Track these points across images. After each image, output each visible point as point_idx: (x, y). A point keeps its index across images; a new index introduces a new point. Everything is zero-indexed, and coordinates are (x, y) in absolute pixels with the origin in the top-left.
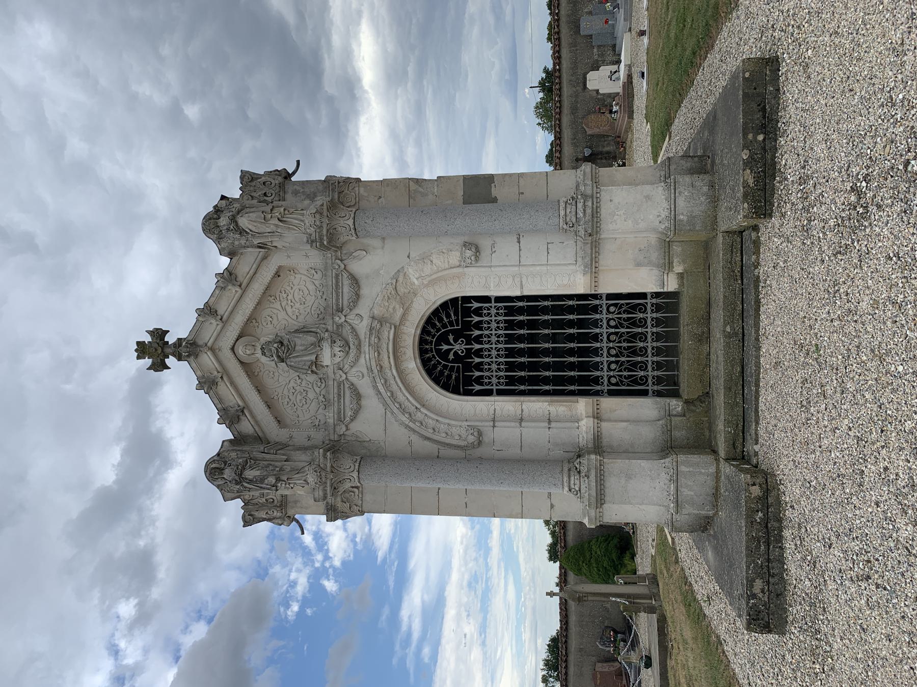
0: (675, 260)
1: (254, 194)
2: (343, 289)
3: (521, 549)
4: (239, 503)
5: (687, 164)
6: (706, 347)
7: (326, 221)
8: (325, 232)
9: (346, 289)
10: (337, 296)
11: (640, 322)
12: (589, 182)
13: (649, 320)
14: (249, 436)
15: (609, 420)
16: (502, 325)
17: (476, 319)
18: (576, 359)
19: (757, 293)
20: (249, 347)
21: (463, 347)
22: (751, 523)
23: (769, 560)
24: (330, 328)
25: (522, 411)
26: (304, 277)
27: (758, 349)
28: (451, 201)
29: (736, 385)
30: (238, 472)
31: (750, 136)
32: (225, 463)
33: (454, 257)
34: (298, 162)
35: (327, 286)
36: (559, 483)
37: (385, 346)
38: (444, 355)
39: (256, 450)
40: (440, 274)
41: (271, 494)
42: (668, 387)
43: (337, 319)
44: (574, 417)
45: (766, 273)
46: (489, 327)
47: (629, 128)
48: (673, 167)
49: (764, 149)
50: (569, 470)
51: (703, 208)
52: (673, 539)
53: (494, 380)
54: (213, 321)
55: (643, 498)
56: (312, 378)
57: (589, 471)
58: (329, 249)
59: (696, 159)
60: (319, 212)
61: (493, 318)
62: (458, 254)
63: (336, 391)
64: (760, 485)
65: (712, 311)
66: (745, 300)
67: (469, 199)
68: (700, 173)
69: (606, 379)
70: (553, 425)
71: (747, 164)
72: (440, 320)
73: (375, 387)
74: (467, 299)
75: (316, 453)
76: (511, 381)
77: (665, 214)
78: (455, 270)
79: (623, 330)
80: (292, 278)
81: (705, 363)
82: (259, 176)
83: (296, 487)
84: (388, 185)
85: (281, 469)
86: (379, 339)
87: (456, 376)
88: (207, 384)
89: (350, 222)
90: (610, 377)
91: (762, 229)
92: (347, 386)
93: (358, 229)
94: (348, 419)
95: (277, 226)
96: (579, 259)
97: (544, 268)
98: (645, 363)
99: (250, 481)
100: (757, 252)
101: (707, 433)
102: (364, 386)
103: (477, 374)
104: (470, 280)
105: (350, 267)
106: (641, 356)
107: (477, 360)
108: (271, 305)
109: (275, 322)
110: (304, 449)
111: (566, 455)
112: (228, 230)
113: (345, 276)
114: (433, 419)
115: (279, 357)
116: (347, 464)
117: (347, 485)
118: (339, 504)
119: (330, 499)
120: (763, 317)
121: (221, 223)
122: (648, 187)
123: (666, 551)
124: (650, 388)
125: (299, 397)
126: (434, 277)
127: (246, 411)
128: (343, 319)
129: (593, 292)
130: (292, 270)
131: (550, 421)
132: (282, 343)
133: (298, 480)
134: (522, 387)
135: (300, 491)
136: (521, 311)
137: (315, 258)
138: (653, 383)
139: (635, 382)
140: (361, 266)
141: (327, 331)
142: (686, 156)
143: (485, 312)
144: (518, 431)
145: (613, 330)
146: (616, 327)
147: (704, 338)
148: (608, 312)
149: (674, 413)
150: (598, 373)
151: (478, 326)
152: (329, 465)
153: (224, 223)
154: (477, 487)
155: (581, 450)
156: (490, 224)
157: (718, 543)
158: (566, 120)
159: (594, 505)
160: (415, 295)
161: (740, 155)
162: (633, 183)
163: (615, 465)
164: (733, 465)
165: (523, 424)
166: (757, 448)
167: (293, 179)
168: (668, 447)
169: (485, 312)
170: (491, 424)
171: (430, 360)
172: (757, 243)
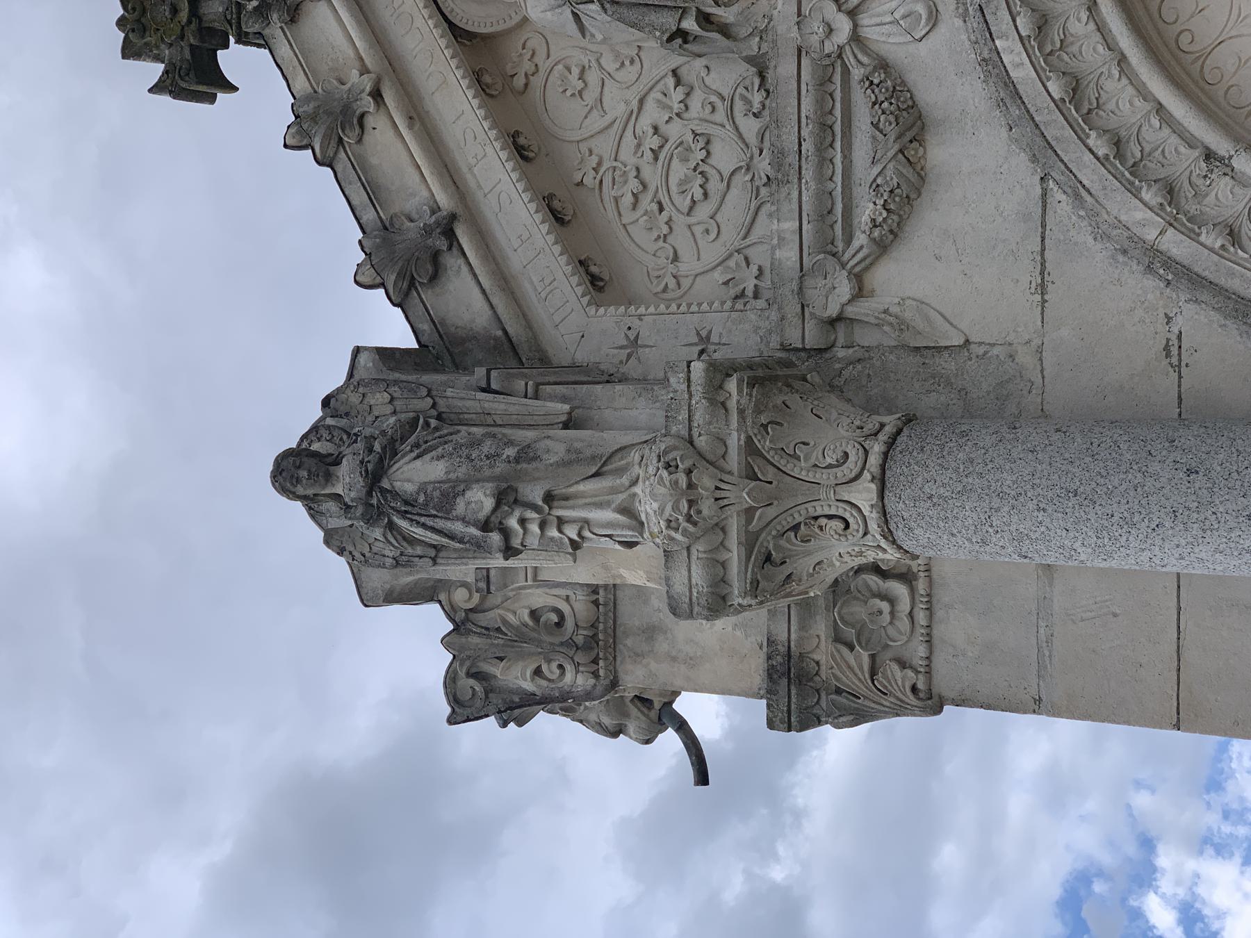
4: (428, 623)
63: (807, 105)
73: (993, 66)
85: (526, 454)
92: (857, 73)
94: (860, 239)
118: (823, 653)
125: (679, 170)
152: (734, 441)
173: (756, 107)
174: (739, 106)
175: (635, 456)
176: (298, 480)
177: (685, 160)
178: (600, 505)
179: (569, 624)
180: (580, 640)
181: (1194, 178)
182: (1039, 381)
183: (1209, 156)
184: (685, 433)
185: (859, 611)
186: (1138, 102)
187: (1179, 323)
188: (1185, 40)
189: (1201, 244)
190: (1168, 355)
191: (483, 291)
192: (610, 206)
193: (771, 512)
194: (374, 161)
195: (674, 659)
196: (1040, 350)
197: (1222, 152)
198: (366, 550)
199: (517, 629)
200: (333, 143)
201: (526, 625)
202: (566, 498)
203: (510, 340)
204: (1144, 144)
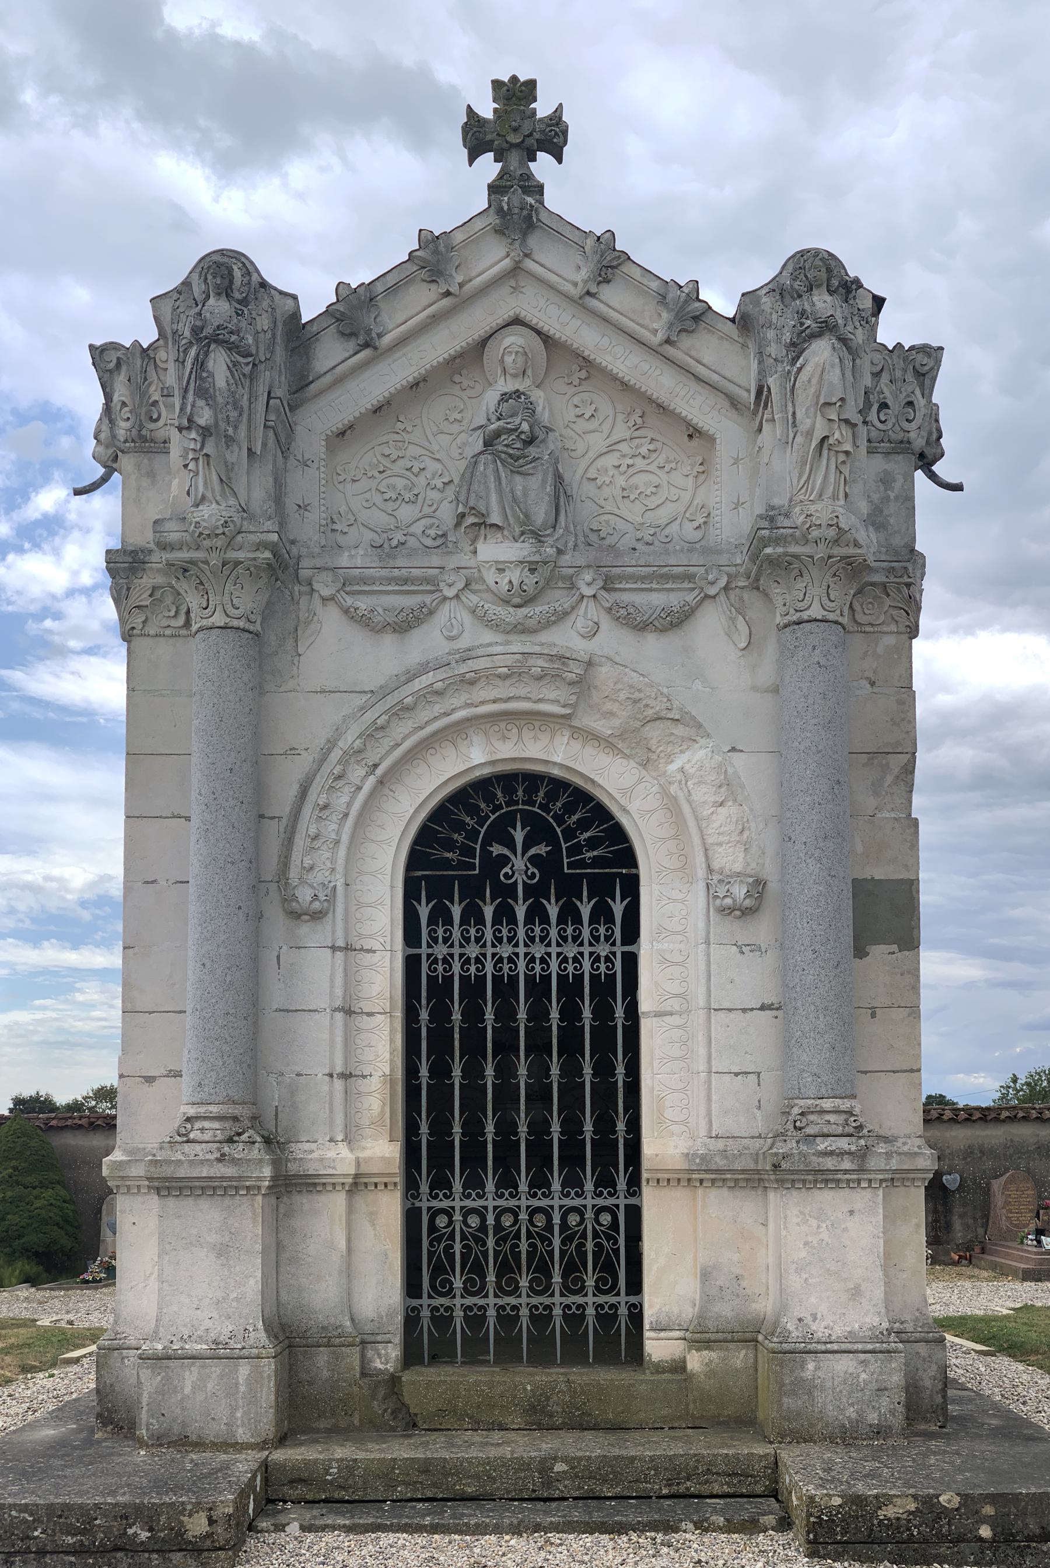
0: (713, 1355)
1: (885, 378)
2: (658, 589)
3: (39, 1015)
4: (148, 334)
5: (928, 1380)
6: (518, 1421)
7: (820, 552)
8: (794, 549)
9: (658, 600)
10: (643, 578)
12: (894, 1164)
13: (579, 1300)
14: (309, 361)
15: (350, 1210)
16: (570, 969)
17: (585, 910)
18: (490, 1138)
19: (640, 1528)
20: (520, 360)
21: (520, 878)
22: (126, 1515)
23: (42, 1553)
24: (566, 559)
25: (370, 1014)
26: (686, 497)
27: (516, 1531)
28: (860, 849)
29: (434, 1485)
30: (224, 335)
31: (989, 1510)
32: (244, 302)
33: (730, 858)
34: (958, 487)
35: (667, 552)
36: (204, 1096)
37: (522, 691)
38: (501, 833)
39: (274, 378)
41: (169, 416)
43: (588, 578)
44: (357, 1134)
45: (686, 1545)
46: (565, 939)
47: (1002, 1272)
48: (922, 1349)
49: (960, 1539)
50: (235, 1119)
51: (831, 1412)
52: (77, 1360)
53: (440, 951)
54: (583, 274)
55: (177, 1285)
56: (447, 514)
57: (235, 1161)
58: (754, 558)
59: (939, 1399)
60: (841, 536)
62: (738, 867)
63: (416, 572)
64: (209, 1535)
65: (601, 1433)
66: (624, 1503)
67: (865, 892)
68: (908, 1407)
69: (445, 1204)
70: (339, 1084)
71: (929, 1503)
72: (584, 825)
73: (425, 668)
74: (632, 888)
75: (268, 525)
77: (819, 1329)
78: (700, 859)
79: (557, 1242)
80: (686, 469)
81: (484, 1420)
82: (927, 391)
83: (187, 476)
84: (901, 702)
85: (230, 440)
86: (540, 678)
88: (433, 257)
89: (816, 612)
90: (448, 1213)
91: (782, 1538)
92: (428, 599)
93: (799, 630)
94: (349, 601)
95: (810, 433)
96: (720, 1144)
97: (702, 1066)
98: (481, 1291)
99: (200, 364)
100: (730, 1528)
101: (323, 1424)
102: (428, 642)
103: (456, 911)
104: (676, 894)
105: (709, 608)
107: (488, 911)
108: (620, 417)
109: (582, 425)
110: (278, 497)
111: (270, 1113)
112: (802, 314)
113: (690, 597)
114: (349, 805)
115: (497, 434)
116: (246, 599)
117: (193, 600)
118: (147, 581)
119: (159, 558)
120: (588, 1539)
121: (820, 294)
122: (879, 1293)
123: (48, 1349)
124: (425, 1301)
127: (366, 353)
128: (588, 591)
129: (645, 1175)
130: (705, 469)
131: (346, 1076)
132: (530, 441)
133: (205, 480)
134: (424, 1015)
135: (177, 485)
136: (603, 1013)
137: (733, 525)
138: (436, 1309)
139: (438, 1270)
140: (711, 627)
141: (560, 552)
142: (946, 1382)
144: (323, 1003)
145: (557, 1220)
146: (564, 1226)
147: (539, 1418)
148: (599, 1211)
149: (370, 1354)
150: (457, 1186)
151: (569, 914)
152: (240, 555)
153: (819, 305)
154: (193, 909)
155: (282, 1146)
156: (807, 942)
157: (75, 1448)
158: (1025, 1132)
159: (157, 1172)
160: (644, 766)
161: (949, 1488)
162: (889, 1262)
163: (248, 1220)
164: (254, 1477)
165: (339, 1016)
166: (294, 1528)
167: (919, 475)
168: (291, 1338)
169: (602, 930)
170: (340, 943)
171: (490, 798)
172: (751, 1527)
173: (428, 532)
174: (430, 521)
175: (232, 502)
176: (214, 277)
177: (405, 488)
178: (205, 483)
179: (152, 426)
180: (144, 432)
182: (281, 690)
183: (376, 766)
184: (243, 529)
185: (169, 600)
186: (402, 735)
187: (304, 754)
188: (432, 751)
191: (334, 367)
192: (384, 439)
193: (208, 573)
194: (411, 290)
195: (138, 490)
196: (294, 690)
198: (181, 310)
199: (147, 391)
200: (422, 264)
201: (149, 398)
202: (208, 464)
203: (307, 385)
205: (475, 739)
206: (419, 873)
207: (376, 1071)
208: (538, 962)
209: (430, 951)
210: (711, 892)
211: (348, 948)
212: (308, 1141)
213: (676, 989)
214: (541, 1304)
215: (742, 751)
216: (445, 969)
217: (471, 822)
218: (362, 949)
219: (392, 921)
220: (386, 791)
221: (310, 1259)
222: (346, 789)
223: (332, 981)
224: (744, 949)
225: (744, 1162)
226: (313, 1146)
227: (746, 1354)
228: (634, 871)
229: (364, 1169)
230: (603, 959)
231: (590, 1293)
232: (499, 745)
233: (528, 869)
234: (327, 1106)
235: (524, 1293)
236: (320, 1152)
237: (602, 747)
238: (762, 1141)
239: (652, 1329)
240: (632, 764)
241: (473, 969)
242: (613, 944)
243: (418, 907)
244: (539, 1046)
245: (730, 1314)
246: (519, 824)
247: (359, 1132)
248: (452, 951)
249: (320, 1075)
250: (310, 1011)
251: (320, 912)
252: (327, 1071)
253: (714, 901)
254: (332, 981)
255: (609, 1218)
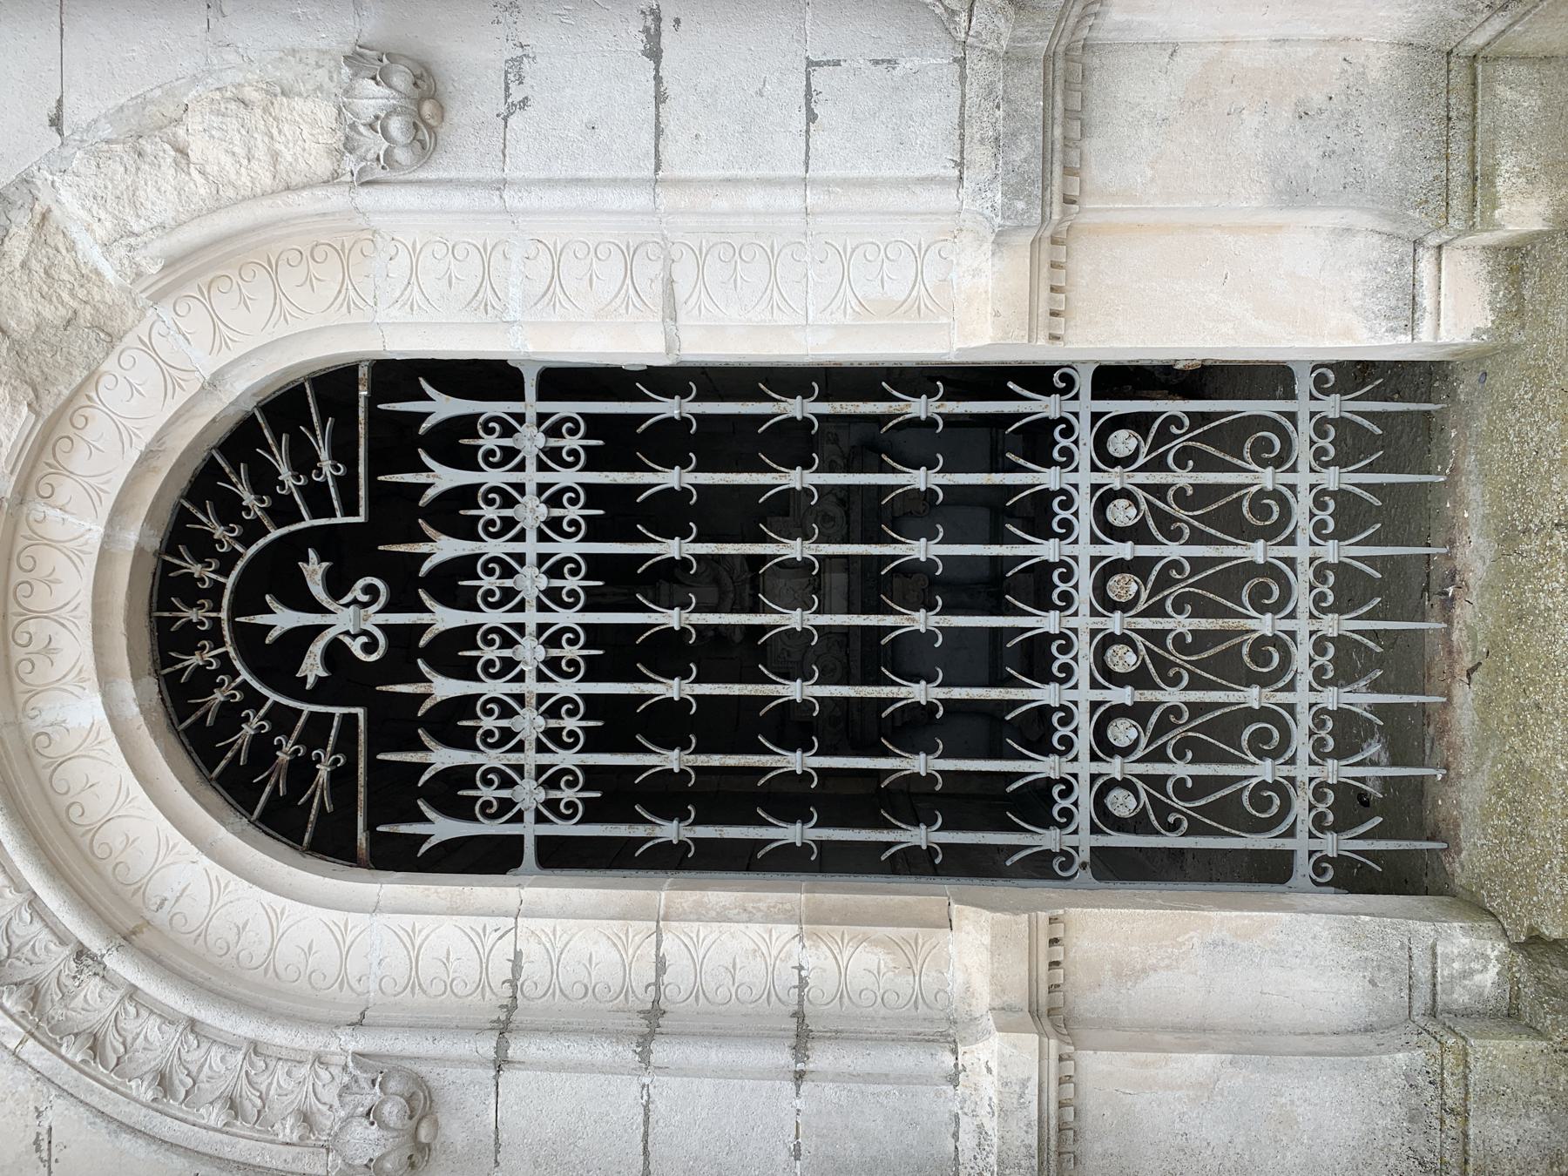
0: (1507, 165)
11: (1261, 510)
21: (374, 619)
25: (661, 966)
38: (278, 658)
40: (223, 222)
42: (1393, 852)
61: (531, 477)
62: (325, 112)
70: (822, 1058)
74: (400, 376)
76: (615, 795)
78: (304, 202)
87: (329, 769)
96: (979, 155)
97: (792, 199)
103: (443, 757)
106: (1264, 681)
107: (444, 688)
114: (168, 1018)
124: (1300, 844)
126: (193, 234)
136: (669, 442)
138: (1318, 821)
143: (489, 442)
144: (627, 1091)
149: (1460, 997)
150: (1046, 767)
151: (454, 513)
160: (112, 339)
165: (661, 1052)
169: (489, 442)
171: (204, 681)
181: (63, 979)
183: (81, 953)
187: (49, 1118)
188: (75, 812)
189: (62, 1057)
190: (38, 1150)
197: (95, 950)
204: (13, 939)
205: (48, 717)
206: (362, 837)
207: (789, 956)
208: (556, 583)
209: (529, 817)
210: (379, 174)
211: (503, 1029)
212: (956, 1136)
213: (613, 269)
214: (1312, 588)
215: (60, 102)
216: (571, 785)
217: (255, 722)
218: (513, 983)
219: (454, 911)
220: (161, 918)
221: (1240, 1140)
222: (130, 1025)
223: (577, 1068)
224: (516, 96)
225: (1027, 93)
226: (966, 1123)
227: (1506, 83)
228: (363, 372)
229: (1019, 997)
230: (554, 442)
231: (1290, 478)
232: (63, 662)
233: (355, 601)
234: (872, 1088)
235: (1288, 625)
236: (984, 1111)
237: (71, 432)
238: (972, 56)
239: (1412, 326)
240: (109, 365)
241: (571, 724)
242: (520, 418)
243: (433, 841)
244: (873, 585)
245: (1394, 132)
246: (261, 619)
247: (930, 998)
248: (530, 769)
249: (798, 1103)
250: (646, 1122)
251: (410, 1100)
252: (790, 1086)
253: (401, 167)
254: (577, 1068)
255: (1122, 434)
